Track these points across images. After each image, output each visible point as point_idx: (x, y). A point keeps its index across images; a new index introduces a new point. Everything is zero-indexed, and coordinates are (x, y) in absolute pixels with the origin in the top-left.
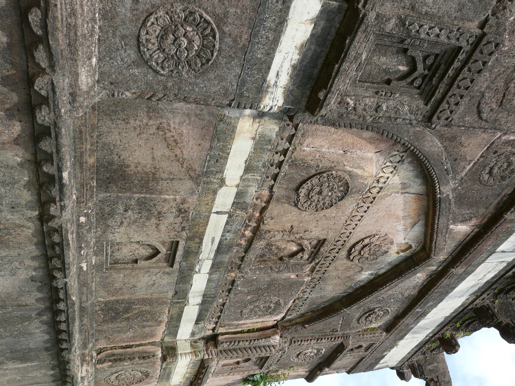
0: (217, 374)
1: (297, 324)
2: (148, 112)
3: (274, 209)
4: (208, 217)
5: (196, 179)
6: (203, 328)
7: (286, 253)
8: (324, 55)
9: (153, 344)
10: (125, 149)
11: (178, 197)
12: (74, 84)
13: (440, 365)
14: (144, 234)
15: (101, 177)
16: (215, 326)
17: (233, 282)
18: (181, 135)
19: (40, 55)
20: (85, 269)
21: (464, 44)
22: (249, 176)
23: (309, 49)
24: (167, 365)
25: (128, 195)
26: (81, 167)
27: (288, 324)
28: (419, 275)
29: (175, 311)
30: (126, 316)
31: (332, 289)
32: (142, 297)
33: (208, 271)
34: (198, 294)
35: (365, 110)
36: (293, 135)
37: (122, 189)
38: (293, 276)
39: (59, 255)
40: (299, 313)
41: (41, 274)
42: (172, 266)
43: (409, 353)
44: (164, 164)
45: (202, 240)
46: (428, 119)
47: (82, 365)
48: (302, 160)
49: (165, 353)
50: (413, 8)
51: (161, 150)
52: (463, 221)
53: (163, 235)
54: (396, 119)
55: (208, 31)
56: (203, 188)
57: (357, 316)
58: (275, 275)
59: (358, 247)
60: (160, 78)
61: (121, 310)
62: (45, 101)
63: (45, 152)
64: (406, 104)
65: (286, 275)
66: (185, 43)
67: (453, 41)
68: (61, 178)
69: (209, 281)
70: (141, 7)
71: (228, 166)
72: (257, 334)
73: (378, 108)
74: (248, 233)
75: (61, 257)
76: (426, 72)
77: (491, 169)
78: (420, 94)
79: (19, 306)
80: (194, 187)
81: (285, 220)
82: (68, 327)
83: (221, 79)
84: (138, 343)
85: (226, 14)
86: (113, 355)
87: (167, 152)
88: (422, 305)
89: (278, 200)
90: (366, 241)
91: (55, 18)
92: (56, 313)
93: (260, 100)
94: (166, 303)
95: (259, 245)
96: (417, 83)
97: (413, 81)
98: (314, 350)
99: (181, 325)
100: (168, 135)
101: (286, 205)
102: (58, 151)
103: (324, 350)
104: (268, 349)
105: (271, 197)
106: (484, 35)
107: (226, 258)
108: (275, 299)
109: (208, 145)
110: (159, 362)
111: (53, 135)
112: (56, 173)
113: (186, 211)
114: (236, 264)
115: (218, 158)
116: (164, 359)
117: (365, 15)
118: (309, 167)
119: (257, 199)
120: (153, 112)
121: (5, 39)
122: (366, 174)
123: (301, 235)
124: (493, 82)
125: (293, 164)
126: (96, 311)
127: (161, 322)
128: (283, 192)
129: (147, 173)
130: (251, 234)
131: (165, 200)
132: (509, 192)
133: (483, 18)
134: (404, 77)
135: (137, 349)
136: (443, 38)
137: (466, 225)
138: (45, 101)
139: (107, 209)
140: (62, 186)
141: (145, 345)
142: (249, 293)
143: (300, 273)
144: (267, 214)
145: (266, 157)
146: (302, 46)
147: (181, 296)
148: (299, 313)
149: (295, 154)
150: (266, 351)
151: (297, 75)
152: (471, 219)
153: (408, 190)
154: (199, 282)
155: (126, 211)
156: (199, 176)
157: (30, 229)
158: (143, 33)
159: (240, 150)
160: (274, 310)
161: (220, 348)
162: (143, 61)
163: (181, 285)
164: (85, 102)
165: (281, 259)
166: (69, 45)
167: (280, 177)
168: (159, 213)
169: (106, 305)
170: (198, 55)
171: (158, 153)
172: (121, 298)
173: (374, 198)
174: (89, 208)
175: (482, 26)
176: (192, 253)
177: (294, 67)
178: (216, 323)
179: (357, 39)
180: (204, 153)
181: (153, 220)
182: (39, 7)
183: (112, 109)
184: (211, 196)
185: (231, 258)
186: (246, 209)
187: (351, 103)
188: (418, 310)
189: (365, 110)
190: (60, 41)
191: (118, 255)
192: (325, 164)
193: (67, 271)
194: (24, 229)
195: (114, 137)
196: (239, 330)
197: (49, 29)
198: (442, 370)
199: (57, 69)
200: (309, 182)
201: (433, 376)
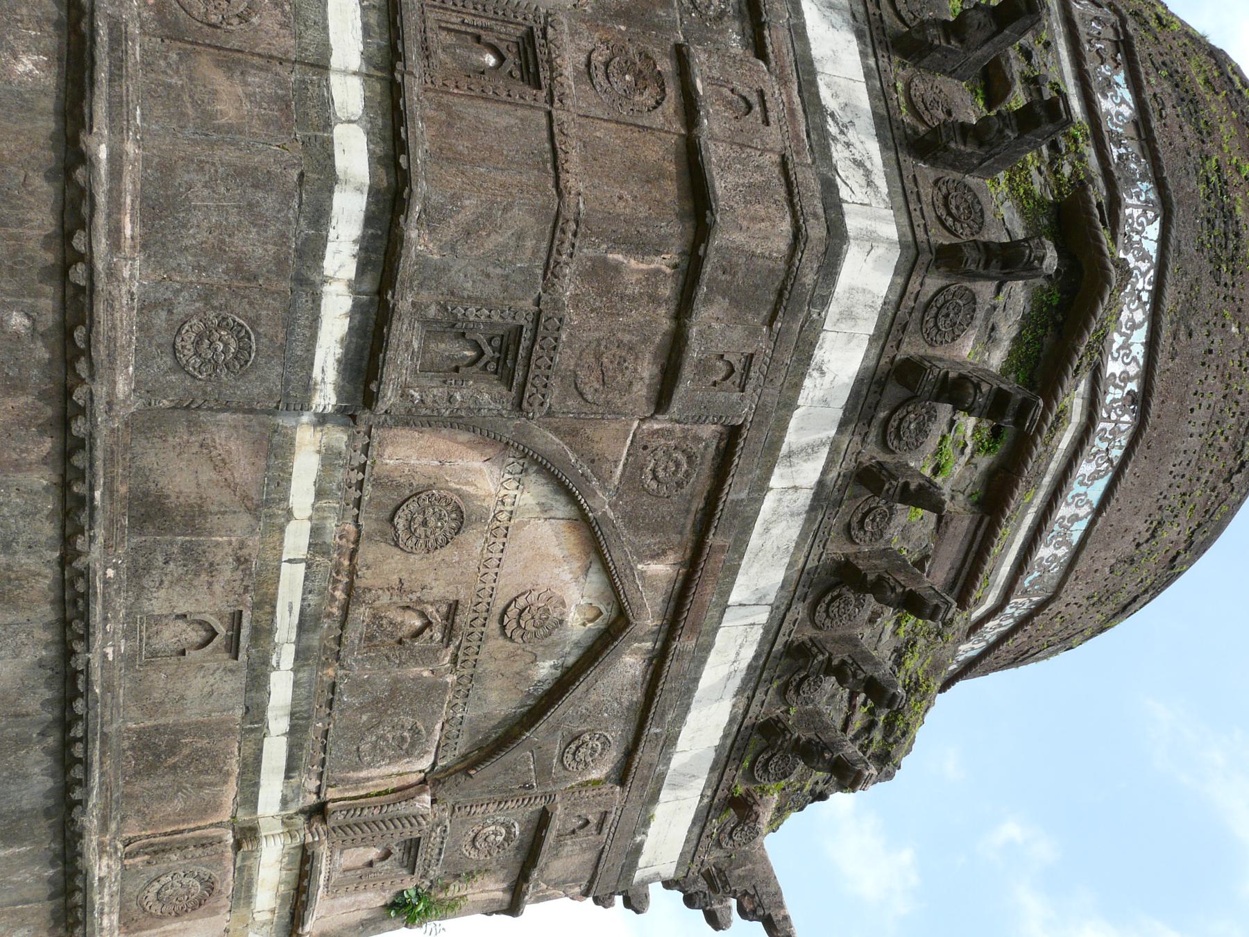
0: (334, 889)
1: (456, 772)
2: (188, 427)
3: (368, 553)
4: (279, 568)
6: (299, 787)
7: (405, 631)
8: (368, 345)
9: (219, 825)
10: (163, 474)
11: (233, 539)
12: (112, 393)
13: (758, 867)
14: (193, 601)
15: (134, 513)
16: (318, 783)
17: (333, 686)
18: (229, 452)
19: (82, 367)
20: (110, 658)
21: (523, 322)
22: (323, 503)
23: (351, 342)
24: (244, 859)
25: (168, 537)
26: (111, 497)
27: (443, 775)
28: (628, 659)
29: (248, 749)
30: (171, 761)
31: (498, 702)
32: (194, 718)
33: (291, 666)
34: (282, 713)
35: (435, 401)
36: (368, 444)
37: (161, 531)
38: (426, 674)
39: (83, 613)
40: (457, 753)
41: (53, 654)
42: (236, 658)
43: (687, 841)
44: (213, 493)
45: (274, 607)
46: (518, 406)
47: (100, 858)
48: (387, 477)
49: (238, 837)
50: (452, 294)
51: (207, 474)
52: (656, 556)
53: (218, 602)
54: (479, 410)
55: (243, 333)
56: (265, 524)
57: (557, 752)
58: (397, 672)
59: (513, 612)
60: (198, 383)
61: (163, 748)
62: (81, 411)
63: (77, 468)
64: (486, 395)
65: (414, 670)
66: (221, 347)
67: (510, 320)
68: (92, 499)
69: (296, 684)
70: (175, 318)
71: (293, 491)
72: (393, 796)
73: (450, 399)
74: (339, 595)
75: (85, 616)
76: (497, 355)
77: (654, 471)
78: (500, 380)
79: (16, 716)
80: (253, 522)
81: (385, 566)
82: (86, 751)
83: (263, 379)
84: (192, 826)
85: (258, 317)
86: (152, 845)
87: (214, 475)
88: (657, 718)
89: (370, 538)
90: (522, 602)
91: (98, 333)
93: (310, 400)
94: (231, 731)
95: (361, 614)
96: (492, 367)
97: (486, 365)
98: (501, 823)
99: (262, 782)
100: (214, 453)
101: (383, 544)
102: (92, 465)
103: (516, 825)
104: (414, 821)
105: (359, 533)
106: (540, 311)
107: (314, 640)
108: (408, 721)
109: (263, 463)
110: (230, 853)
111: (87, 447)
112: (87, 493)
113: (246, 561)
114: (332, 650)
115: (281, 480)
116: (238, 846)
117: (394, 305)
118: (399, 486)
119: (341, 538)
120: (193, 426)
121: (47, 356)
122: (481, 493)
123: (418, 594)
124: (580, 358)
125: (377, 483)
126: (124, 751)
127: (228, 774)
128: (374, 526)
129: (191, 506)
130: (344, 596)
131: (217, 544)
132: (701, 506)
133: (535, 296)
134: (474, 362)
135: (191, 834)
136: (496, 318)
137: (662, 562)
138: (81, 411)
139: (142, 561)
140: (93, 508)
141: (205, 827)
142: (362, 709)
143: (435, 666)
144: (359, 560)
145: (340, 475)
146: (342, 340)
147: (255, 713)
148: (457, 753)
149: (376, 469)
150: (412, 825)
151: (345, 370)
152: (664, 552)
153: (552, 514)
154: (281, 688)
155: (166, 563)
156: (258, 506)
157: (45, 581)
158: (178, 340)
159: (305, 468)
160: (413, 745)
161: (331, 823)
162: (180, 367)
163: (253, 694)
164: (122, 412)
165: (400, 642)
166: (108, 355)
167: (364, 504)
168: (211, 564)
169: (139, 738)
170: (236, 358)
171: (204, 478)
172: (162, 721)
173: (507, 529)
174: (119, 558)
175: (538, 302)
176: (263, 632)
177: (339, 361)
178: (320, 776)
179: (394, 327)
180: (260, 475)
181: (204, 577)
182: (84, 324)
183: (147, 423)
184: (277, 536)
185: (321, 639)
186: (328, 553)
187: (416, 395)
188: (654, 730)
189: (435, 401)
190: (100, 353)
191: (157, 643)
192: (419, 481)
193: (91, 639)
194: (40, 579)
196: (362, 793)
197: (92, 342)
198: (761, 875)
199: (97, 378)
200: (404, 506)
201: (747, 886)
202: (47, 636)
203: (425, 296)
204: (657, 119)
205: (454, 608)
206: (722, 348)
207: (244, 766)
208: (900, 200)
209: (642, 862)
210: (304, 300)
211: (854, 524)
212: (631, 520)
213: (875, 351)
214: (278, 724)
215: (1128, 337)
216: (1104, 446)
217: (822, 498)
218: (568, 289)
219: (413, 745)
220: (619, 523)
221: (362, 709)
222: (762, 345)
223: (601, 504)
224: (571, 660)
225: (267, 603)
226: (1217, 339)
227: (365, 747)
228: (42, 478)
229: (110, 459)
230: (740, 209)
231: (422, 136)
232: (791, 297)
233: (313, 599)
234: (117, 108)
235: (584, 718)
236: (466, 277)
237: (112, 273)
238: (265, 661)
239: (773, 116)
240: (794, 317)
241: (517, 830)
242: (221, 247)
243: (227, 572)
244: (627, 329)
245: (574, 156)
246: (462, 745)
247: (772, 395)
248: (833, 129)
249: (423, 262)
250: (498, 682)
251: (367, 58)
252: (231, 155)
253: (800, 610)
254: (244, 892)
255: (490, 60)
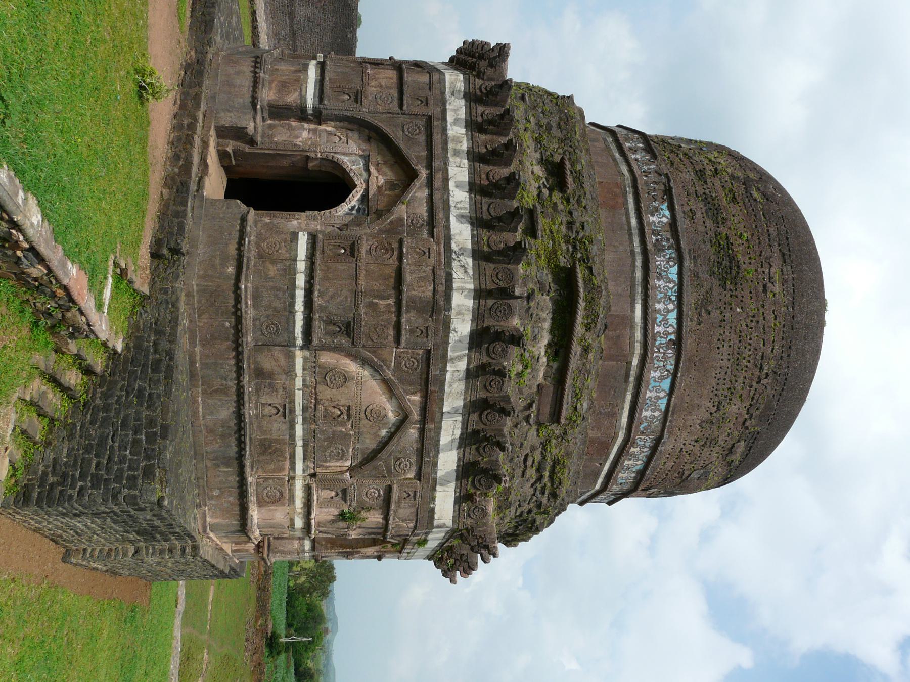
3: (320, 388)
5: (287, 374)
17: (314, 432)
31: (370, 443)
37: (263, 379)
43: (454, 511)
44: (275, 368)
51: (273, 363)
52: (413, 393)
64: (344, 341)
65: (340, 428)
69: (304, 429)
74: (313, 401)
81: (326, 393)
90: (371, 407)
92: (240, 436)
94: (285, 443)
95: (321, 407)
115: (293, 365)
116: (288, 481)
142: (325, 440)
145: (309, 364)
147: (292, 437)
154: (299, 430)
160: (343, 455)
176: (292, 411)
190: (244, 331)
195: (259, 359)
202: (234, 404)
203: (322, 314)
204: (391, 261)
205: (349, 407)
206: (416, 325)
207: (290, 455)
208: (477, 276)
209: (436, 517)
210: (291, 317)
211: (487, 384)
212: (401, 381)
213: (474, 325)
214: (299, 443)
215: (666, 316)
216: (662, 364)
217: (470, 375)
218: (362, 310)
219: (343, 455)
220: (396, 382)
221: (325, 440)
222: (431, 324)
223: (389, 374)
224: (393, 430)
225: (292, 402)
226: (728, 315)
227: (327, 454)
228: (233, 362)
229: (249, 358)
230: (415, 285)
231: (319, 274)
232: (437, 308)
233: (306, 402)
234: (247, 276)
235: (400, 452)
236: (332, 308)
237: (246, 312)
238: (294, 421)
239: (432, 255)
240: (440, 315)
241: (382, 492)
242: (270, 305)
243: (281, 392)
244: (382, 320)
245: (363, 275)
246: (359, 459)
247: (439, 340)
248: (454, 256)
249: (320, 306)
250: (368, 436)
251: (307, 256)
252: (271, 284)
253: (475, 417)
254: (292, 499)
255: (343, 251)
